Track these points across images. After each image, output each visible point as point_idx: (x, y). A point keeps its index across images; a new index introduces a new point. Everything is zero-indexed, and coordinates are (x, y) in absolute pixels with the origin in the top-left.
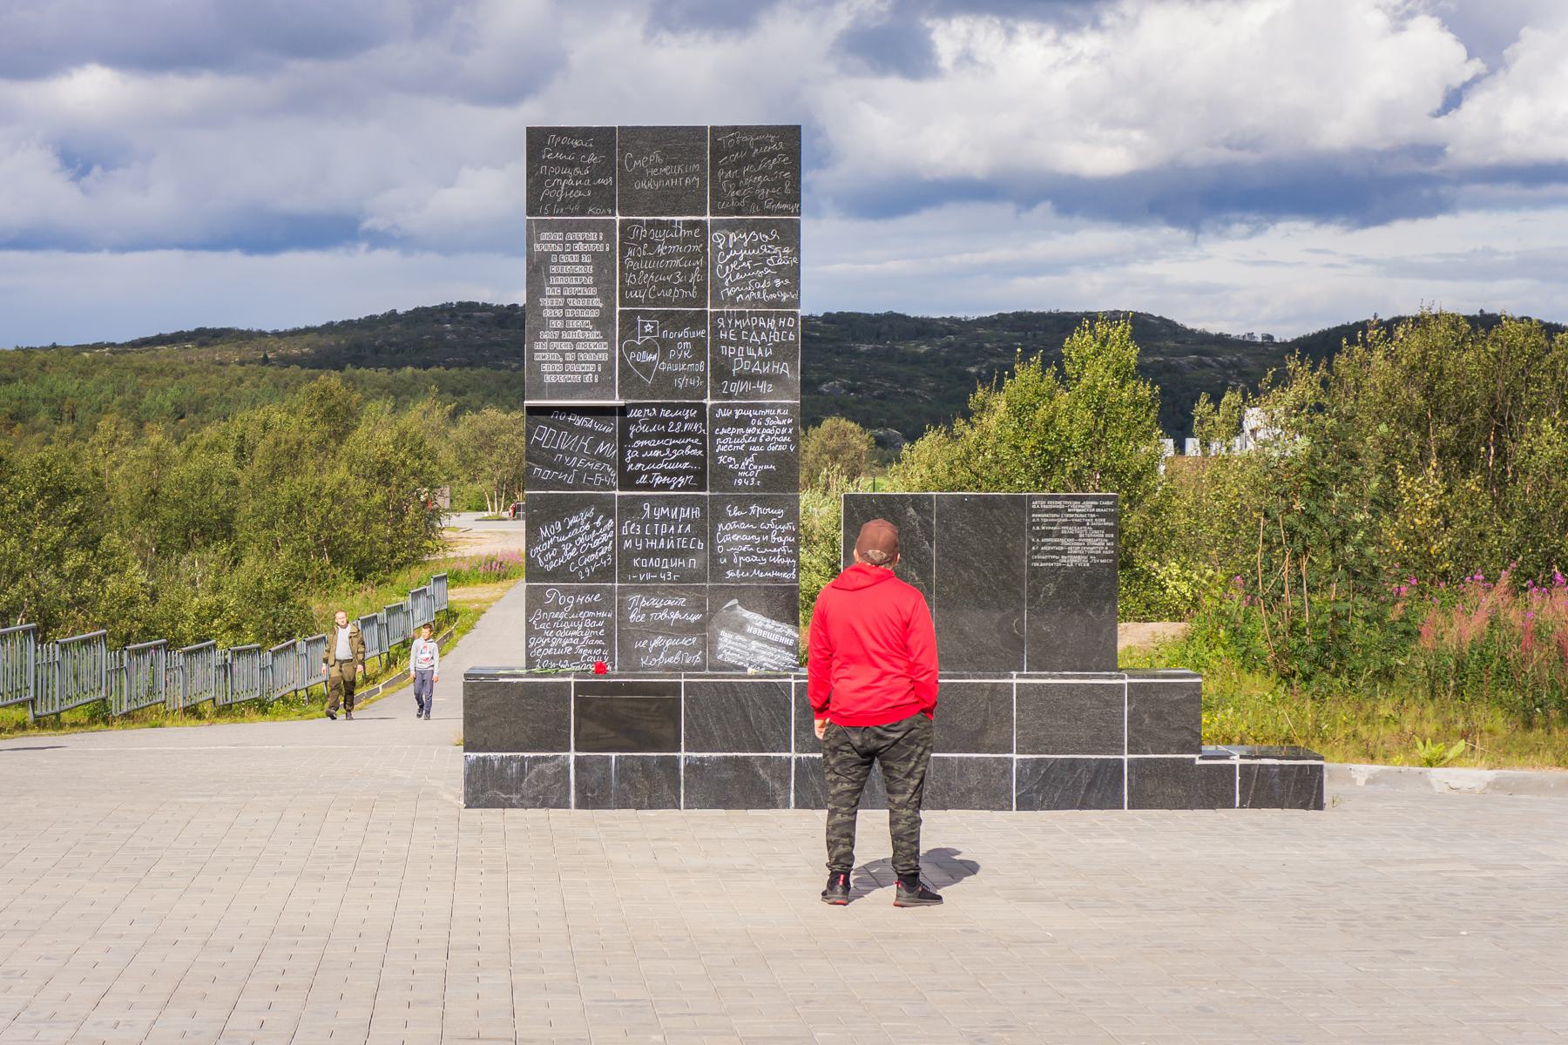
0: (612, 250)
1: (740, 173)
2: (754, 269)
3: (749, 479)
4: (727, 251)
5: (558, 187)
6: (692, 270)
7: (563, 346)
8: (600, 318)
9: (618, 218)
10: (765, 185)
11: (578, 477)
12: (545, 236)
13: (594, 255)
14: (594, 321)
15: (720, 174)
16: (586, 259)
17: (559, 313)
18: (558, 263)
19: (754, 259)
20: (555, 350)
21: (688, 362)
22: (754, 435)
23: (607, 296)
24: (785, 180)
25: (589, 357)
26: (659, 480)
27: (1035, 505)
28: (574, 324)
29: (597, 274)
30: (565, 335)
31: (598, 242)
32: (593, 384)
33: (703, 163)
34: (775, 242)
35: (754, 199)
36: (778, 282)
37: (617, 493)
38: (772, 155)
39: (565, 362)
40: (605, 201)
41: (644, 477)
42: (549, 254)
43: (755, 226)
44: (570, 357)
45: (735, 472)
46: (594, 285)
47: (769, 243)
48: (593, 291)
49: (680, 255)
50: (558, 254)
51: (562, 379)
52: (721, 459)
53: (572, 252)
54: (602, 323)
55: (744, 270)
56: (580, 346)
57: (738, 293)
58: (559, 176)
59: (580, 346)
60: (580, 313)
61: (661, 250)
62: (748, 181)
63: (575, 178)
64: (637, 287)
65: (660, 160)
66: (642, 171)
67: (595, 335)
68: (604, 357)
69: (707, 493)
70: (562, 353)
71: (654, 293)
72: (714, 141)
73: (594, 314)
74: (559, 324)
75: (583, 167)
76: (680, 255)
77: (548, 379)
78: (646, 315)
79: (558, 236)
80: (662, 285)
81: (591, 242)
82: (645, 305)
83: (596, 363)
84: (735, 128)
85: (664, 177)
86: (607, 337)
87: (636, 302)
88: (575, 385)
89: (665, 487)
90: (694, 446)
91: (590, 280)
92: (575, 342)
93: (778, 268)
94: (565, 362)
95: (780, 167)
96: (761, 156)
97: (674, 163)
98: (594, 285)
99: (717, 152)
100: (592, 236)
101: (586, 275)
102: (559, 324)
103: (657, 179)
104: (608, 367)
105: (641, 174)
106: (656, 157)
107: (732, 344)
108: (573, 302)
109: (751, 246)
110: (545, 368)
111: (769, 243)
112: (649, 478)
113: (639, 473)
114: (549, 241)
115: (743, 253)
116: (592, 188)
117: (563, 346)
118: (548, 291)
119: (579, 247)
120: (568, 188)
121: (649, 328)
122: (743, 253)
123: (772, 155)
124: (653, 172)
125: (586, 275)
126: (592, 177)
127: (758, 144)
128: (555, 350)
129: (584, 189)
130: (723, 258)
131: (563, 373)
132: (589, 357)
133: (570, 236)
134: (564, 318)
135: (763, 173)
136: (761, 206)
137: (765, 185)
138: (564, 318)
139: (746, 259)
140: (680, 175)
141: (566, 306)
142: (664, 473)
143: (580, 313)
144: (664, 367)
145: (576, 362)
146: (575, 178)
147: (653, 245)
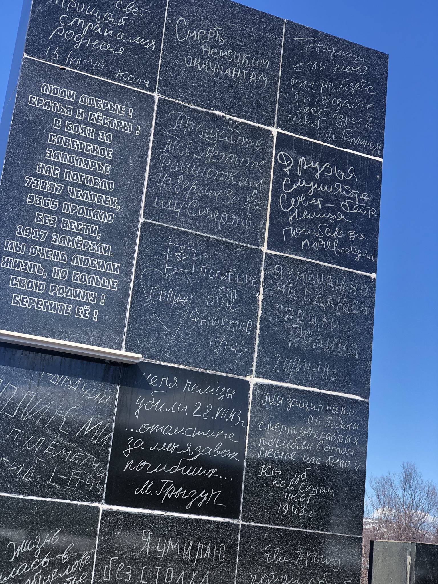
0: (144, 136)
1: (316, 87)
2: (326, 210)
3: (298, 506)
4: (294, 178)
5: (77, 29)
6: (248, 191)
7: (51, 255)
8: (115, 226)
9: (157, 96)
10: (344, 111)
11: (42, 472)
12: (47, 88)
13: (118, 135)
14: (104, 228)
15: (294, 80)
16: (103, 137)
17: (52, 204)
18: (62, 132)
19: (326, 198)
20: (37, 259)
21: (231, 317)
22: (310, 439)
23: (128, 192)
24: (367, 112)
25: (90, 281)
26: (169, 492)
27: (16, 282)
28: (75, 226)
29: (119, 161)
30: (56, 239)
31: (125, 118)
32: (89, 323)
33: (274, 63)
34: (351, 183)
35: (330, 123)
36: (352, 235)
37: (103, 506)
38: (355, 78)
39: (50, 280)
40: (142, 66)
41: (148, 485)
42: (50, 116)
43: (328, 156)
44: (59, 273)
45: (279, 493)
46: (113, 177)
47: (344, 182)
48: (108, 185)
49: (235, 167)
50: (64, 119)
51: (41, 305)
52: (263, 470)
53: (85, 123)
54: (117, 234)
55: (312, 209)
56: (77, 261)
57: (303, 237)
58: (82, 15)
59: (77, 261)
60: (85, 212)
61: (210, 154)
62: (325, 100)
63: (105, 26)
64: (172, 196)
65: (221, 40)
66: (198, 46)
67: (103, 249)
68: (111, 285)
69: (238, 522)
70: (48, 265)
71: (195, 209)
72: (289, 39)
73: (105, 218)
74: (51, 220)
75: (117, 15)
76: (235, 167)
77: (22, 302)
78: (181, 238)
79: (69, 94)
80: (206, 201)
81: (117, 115)
82: (179, 223)
83: (99, 291)
84: (315, 33)
85: (224, 62)
86: (121, 255)
87: (168, 216)
88: (62, 319)
89: (177, 504)
90: (227, 445)
91: (106, 170)
92: (70, 252)
93: (352, 216)
94: (50, 280)
95: (362, 94)
96: (342, 75)
97: (238, 49)
98: (113, 177)
99: (292, 54)
100: (119, 109)
101: (103, 160)
102: (51, 220)
103: (214, 61)
104: (116, 301)
105: (194, 48)
106: (216, 33)
107: (291, 303)
108: (78, 194)
109: (324, 180)
110: (16, 282)
111: (344, 182)
112: (156, 487)
113: (140, 478)
114: (52, 97)
115: (313, 187)
116: (126, 45)
117: (51, 255)
118: (41, 168)
119: (97, 118)
120: (92, 35)
121: (181, 256)
122: (313, 187)
123: (355, 78)
124: (211, 51)
125: (103, 160)
126: (131, 34)
127: (340, 60)
128: (37, 259)
129: (114, 43)
130: (288, 186)
131: (45, 296)
132: (90, 281)
133: (86, 100)
134: (58, 213)
135: (343, 95)
136: (338, 135)
137: (344, 111)
138: (58, 213)
139: (316, 195)
140: (244, 67)
141: (64, 197)
142: (180, 481)
143: (85, 212)
144: (195, 316)
145: (68, 283)
146: (105, 26)
147: (201, 145)
